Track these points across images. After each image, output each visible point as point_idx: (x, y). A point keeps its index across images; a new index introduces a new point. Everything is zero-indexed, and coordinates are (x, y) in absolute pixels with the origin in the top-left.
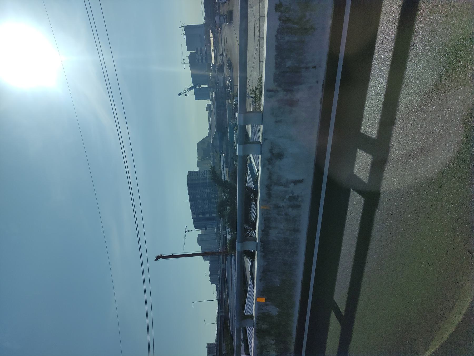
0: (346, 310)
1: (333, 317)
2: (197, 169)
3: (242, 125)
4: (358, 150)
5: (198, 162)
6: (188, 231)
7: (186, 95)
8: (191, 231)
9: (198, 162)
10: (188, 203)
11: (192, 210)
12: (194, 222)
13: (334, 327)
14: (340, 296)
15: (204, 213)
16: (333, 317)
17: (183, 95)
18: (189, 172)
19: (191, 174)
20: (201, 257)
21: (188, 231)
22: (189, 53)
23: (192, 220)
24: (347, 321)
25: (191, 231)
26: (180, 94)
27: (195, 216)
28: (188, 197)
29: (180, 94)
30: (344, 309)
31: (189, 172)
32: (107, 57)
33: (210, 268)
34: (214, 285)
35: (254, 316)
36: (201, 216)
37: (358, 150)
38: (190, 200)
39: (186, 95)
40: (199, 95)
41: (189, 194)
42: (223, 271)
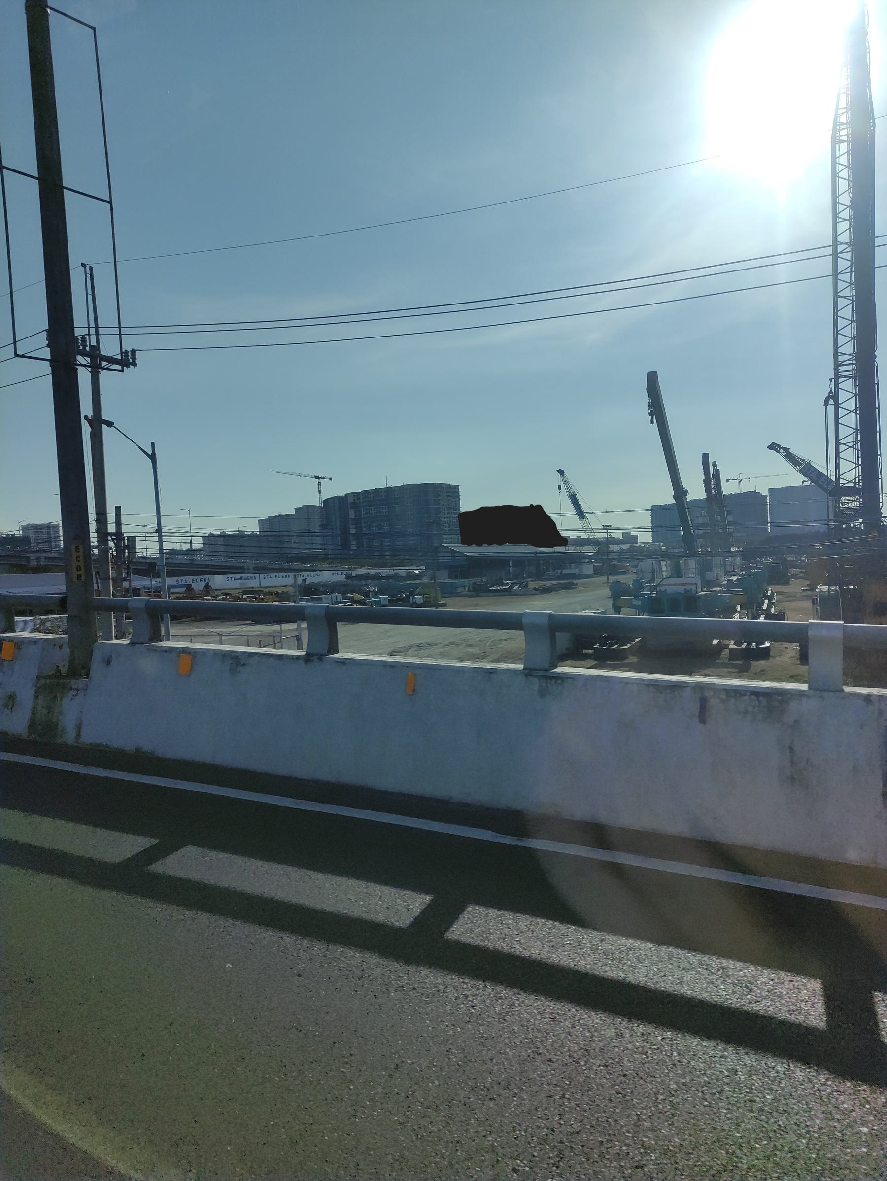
0: (156, 876)
1: (142, 842)
4: (428, 898)
6: (319, 483)
7: (560, 487)
8: (320, 491)
10: (381, 485)
11: (366, 493)
12: (339, 498)
13: (118, 846)
14: (190, 863)
15: (357, 522)
16: (142, 842)
17: (558, 479)
18: (456, 488)
19: (453, 492)
20: (667, 498)
21: (319, 483)
22: (765, 492)
23: (358, 490)
25: (320, 491)
26: (561, 472)
27: (351, 500)
28: (395, 483)
29: (561, 472)
31: (456, 488)
32: (782, 273)
35: (157, 644)
36: (352, 514)
37: (428, 898)
38: (389, 490)
39: (560, 487)
40: (673, 517)
41: (403, 487)
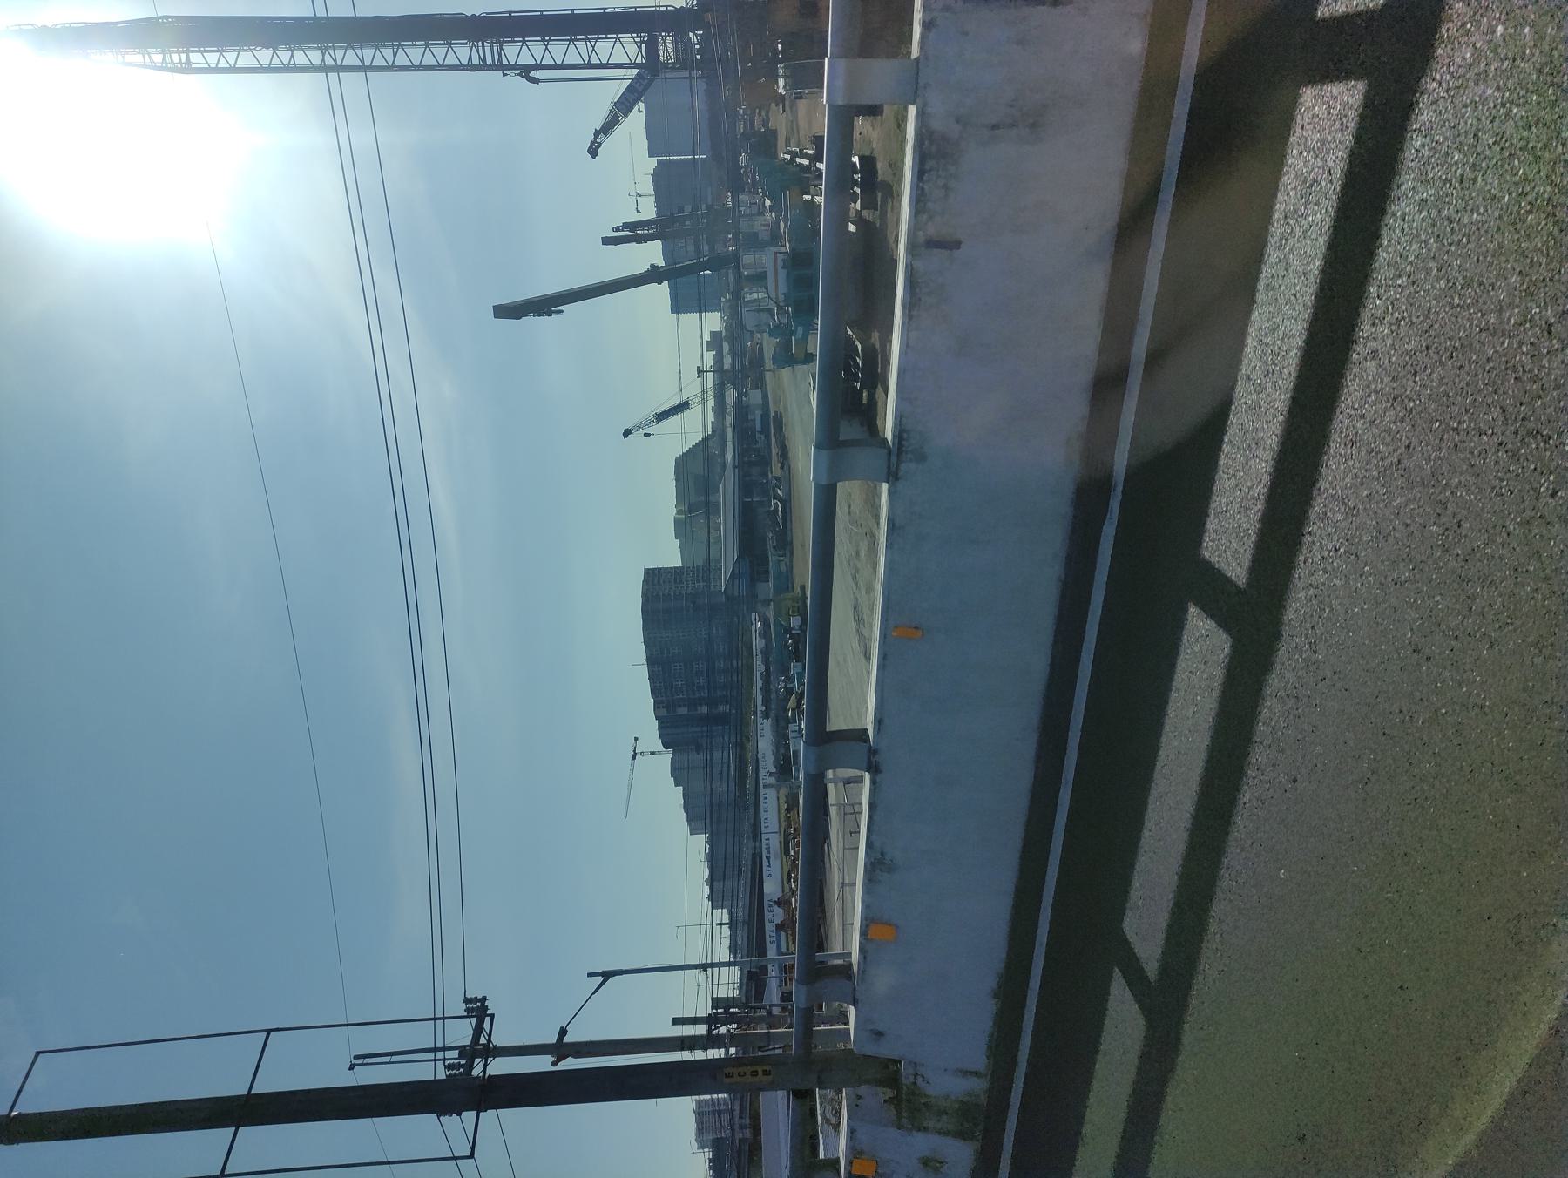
0: (1164, 969)
2: (678, 563)
3: (824, 482)
4: (1193, 609)
5: (677, 521)
6: (642, 754)
7: (647, 435)
8: (652, 753)
9: (678, 523)
13: (1124, 1022)
14: (1145, 926)
17: (637, 436)
18: (647, 572)
19: (654, 579)
21: (642, 754)
22: (653, 162)
24: (1166, 1002)
25: (652, 753)
26: (627, 433)
27: (664, 712)
29: (627, 433)
30: (1157, 952)
31: (647, 572)
33: (712, 859)
34: (723, 915)
37: (1193, 609)
38: (651, 661)
39: (647, 435)
40: (686, 283)
42: (754, 863)
